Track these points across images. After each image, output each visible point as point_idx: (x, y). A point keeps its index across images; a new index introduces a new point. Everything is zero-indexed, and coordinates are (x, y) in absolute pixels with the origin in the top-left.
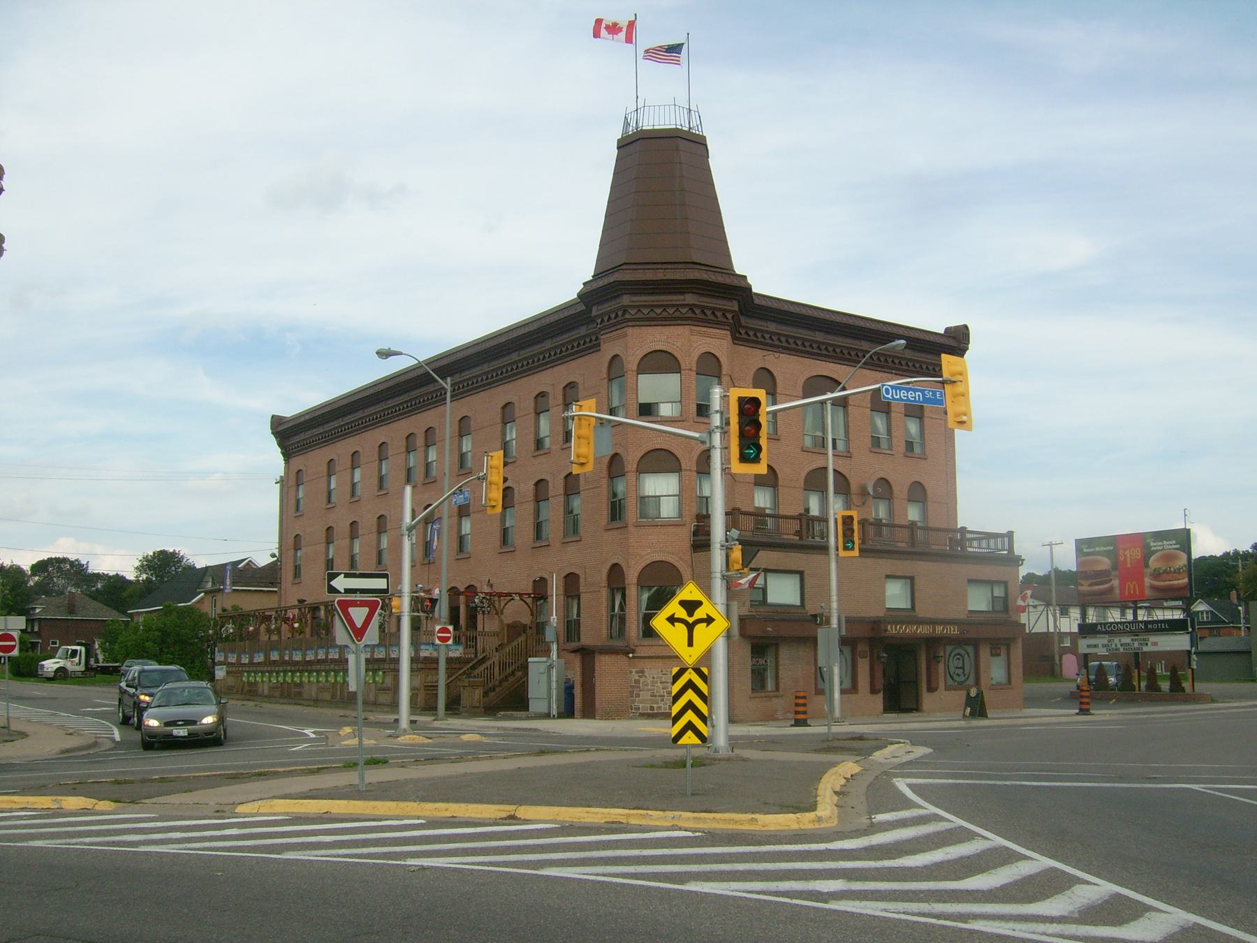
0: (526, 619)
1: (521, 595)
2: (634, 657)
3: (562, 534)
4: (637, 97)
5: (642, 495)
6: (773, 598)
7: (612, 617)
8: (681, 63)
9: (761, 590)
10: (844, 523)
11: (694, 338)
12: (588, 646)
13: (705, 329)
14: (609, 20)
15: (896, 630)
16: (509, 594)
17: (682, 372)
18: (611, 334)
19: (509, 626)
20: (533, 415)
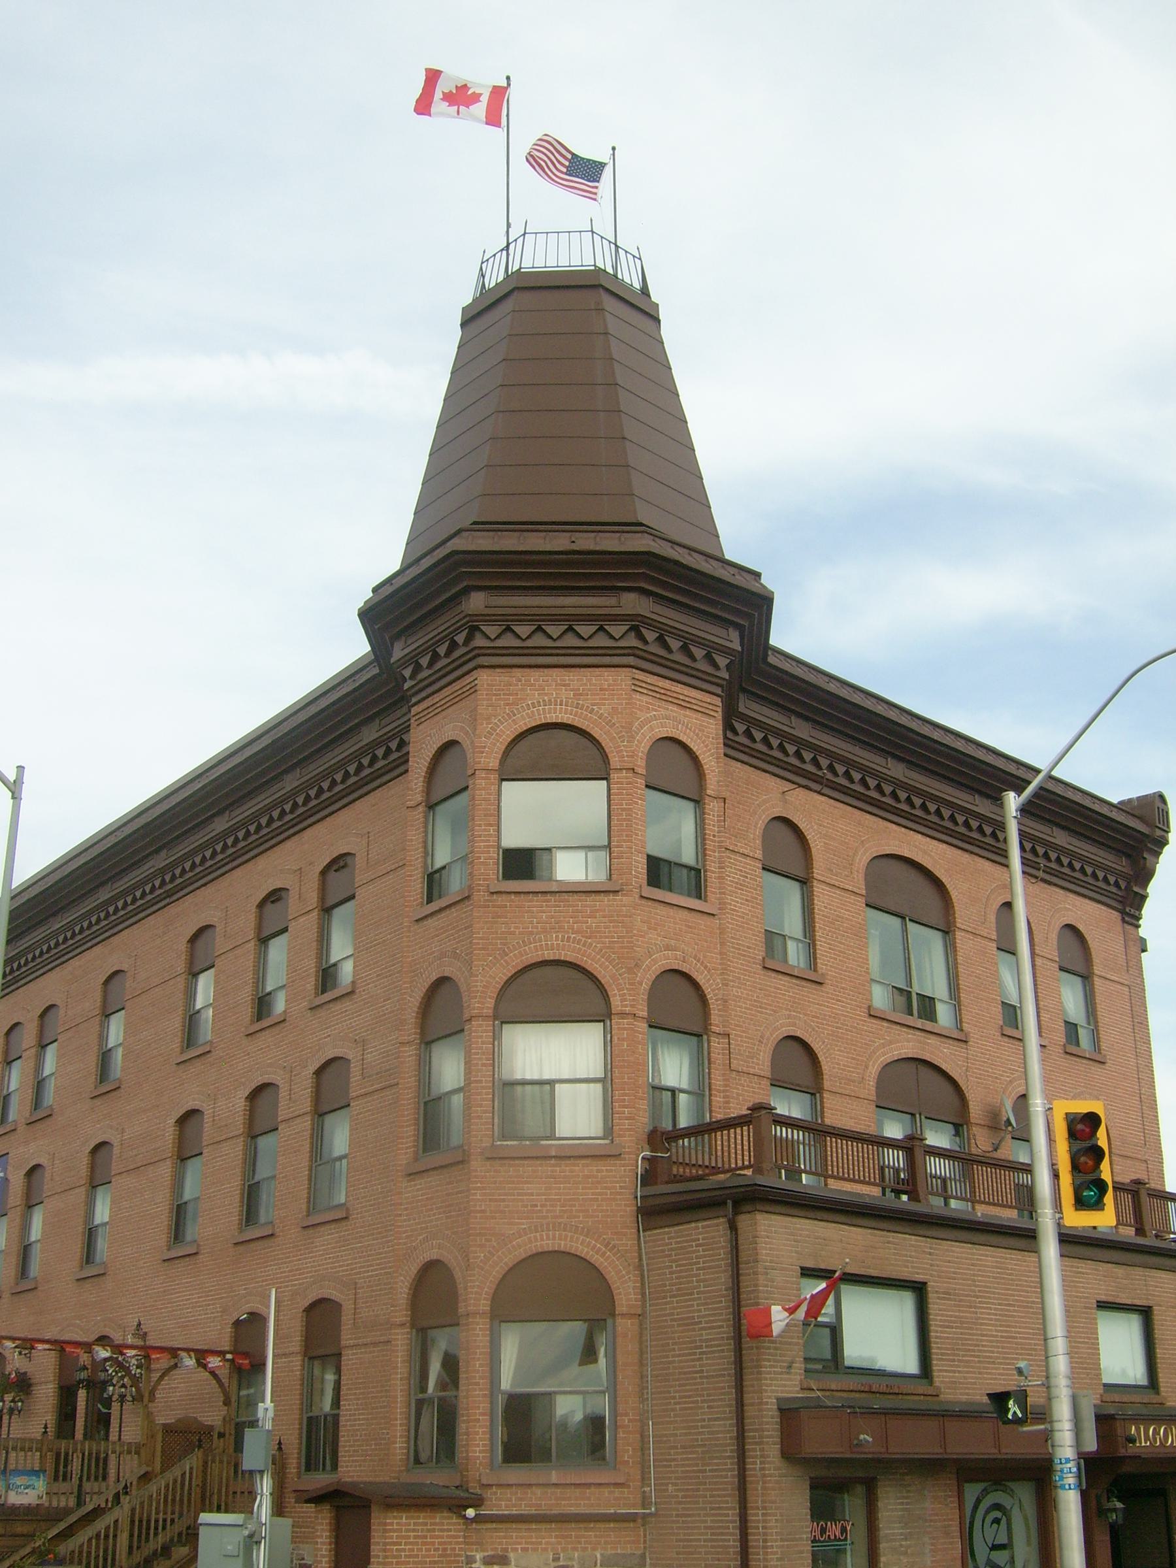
0: (213, 1416)
1: (201, 1355)
2: (478, 1519)
3: (304, 1206)
4: (509, 225)
5: (506, 1076)
6: (855, 1350)
7: (420, 1403)
8: (598, 197)
9: (827, 1331)
10: (1072, 1134)
11: (641, 700)
12: (355, 1484)
13: (667, 684)
14: (455, 72)
15: (1147, 1438)
16: (174, 1352)
17: (614, 776)
18: (436, 698)
19: (168, 1430)
20: (251, 945)
